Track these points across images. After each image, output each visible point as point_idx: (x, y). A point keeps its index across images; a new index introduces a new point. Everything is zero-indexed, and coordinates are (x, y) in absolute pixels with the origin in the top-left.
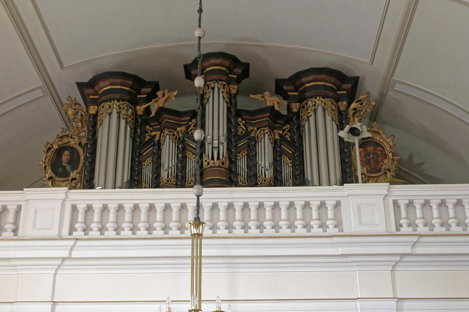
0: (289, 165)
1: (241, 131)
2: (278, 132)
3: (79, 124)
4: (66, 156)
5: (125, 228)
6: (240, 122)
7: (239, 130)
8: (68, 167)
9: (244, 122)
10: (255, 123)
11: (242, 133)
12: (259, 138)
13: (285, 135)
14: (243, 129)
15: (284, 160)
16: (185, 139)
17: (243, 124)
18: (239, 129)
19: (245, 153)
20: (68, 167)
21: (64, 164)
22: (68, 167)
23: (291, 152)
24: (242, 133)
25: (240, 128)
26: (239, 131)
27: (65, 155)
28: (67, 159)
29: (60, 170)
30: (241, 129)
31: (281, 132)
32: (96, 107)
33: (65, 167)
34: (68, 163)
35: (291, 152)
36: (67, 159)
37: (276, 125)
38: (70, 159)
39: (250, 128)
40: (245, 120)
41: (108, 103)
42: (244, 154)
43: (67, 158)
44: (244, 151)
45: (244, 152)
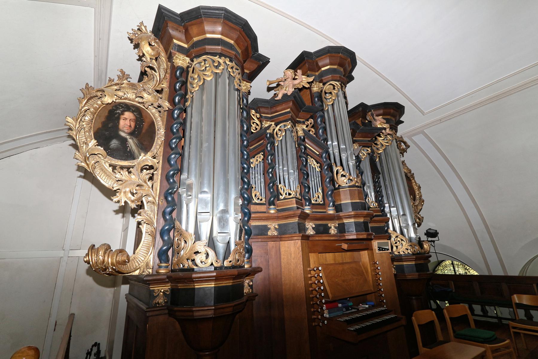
0: (317, 169)
1: (255, 127)
2: (300, 129)
3: (156, 74)
4: (128, 120)
5: (212, 306)
6: (254, 115)
7: (252, 126)
8: (130, 141)
9: (258, 115)
10: (272, 117)
11: (256, 129)
12: (279, 136)
13: (309, 131)
14: (257, 125)
15: (310, 164)
16: (262, 115)
17: (258, 118)
18: (252, 125)
19: (260, 158)
20: (132, 143)
21: (123, 134)
22: (132, 143)
23: (318, 153)
24: (256, 129)
25: (253, 123)
26: (252, 127)
27: (126, 119)
28: (130, 126)
29: (114, 143)
30: (255, 124)
31: (304, 127)
32: (188, 60)
33: (124, 141)
34: (131, 134)
35: (318, 153)
36: (130, 126)
37: (297, 119)
38: (135, 127)
39: (266, 124)
40: (260, 113)
41: (216, 57)
42: (259, 160)
43: (129, 125)
44: (259, 155)
45: (259, 157)
